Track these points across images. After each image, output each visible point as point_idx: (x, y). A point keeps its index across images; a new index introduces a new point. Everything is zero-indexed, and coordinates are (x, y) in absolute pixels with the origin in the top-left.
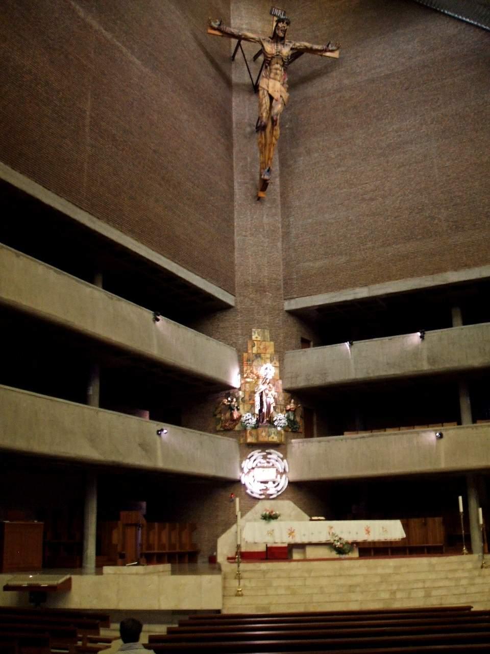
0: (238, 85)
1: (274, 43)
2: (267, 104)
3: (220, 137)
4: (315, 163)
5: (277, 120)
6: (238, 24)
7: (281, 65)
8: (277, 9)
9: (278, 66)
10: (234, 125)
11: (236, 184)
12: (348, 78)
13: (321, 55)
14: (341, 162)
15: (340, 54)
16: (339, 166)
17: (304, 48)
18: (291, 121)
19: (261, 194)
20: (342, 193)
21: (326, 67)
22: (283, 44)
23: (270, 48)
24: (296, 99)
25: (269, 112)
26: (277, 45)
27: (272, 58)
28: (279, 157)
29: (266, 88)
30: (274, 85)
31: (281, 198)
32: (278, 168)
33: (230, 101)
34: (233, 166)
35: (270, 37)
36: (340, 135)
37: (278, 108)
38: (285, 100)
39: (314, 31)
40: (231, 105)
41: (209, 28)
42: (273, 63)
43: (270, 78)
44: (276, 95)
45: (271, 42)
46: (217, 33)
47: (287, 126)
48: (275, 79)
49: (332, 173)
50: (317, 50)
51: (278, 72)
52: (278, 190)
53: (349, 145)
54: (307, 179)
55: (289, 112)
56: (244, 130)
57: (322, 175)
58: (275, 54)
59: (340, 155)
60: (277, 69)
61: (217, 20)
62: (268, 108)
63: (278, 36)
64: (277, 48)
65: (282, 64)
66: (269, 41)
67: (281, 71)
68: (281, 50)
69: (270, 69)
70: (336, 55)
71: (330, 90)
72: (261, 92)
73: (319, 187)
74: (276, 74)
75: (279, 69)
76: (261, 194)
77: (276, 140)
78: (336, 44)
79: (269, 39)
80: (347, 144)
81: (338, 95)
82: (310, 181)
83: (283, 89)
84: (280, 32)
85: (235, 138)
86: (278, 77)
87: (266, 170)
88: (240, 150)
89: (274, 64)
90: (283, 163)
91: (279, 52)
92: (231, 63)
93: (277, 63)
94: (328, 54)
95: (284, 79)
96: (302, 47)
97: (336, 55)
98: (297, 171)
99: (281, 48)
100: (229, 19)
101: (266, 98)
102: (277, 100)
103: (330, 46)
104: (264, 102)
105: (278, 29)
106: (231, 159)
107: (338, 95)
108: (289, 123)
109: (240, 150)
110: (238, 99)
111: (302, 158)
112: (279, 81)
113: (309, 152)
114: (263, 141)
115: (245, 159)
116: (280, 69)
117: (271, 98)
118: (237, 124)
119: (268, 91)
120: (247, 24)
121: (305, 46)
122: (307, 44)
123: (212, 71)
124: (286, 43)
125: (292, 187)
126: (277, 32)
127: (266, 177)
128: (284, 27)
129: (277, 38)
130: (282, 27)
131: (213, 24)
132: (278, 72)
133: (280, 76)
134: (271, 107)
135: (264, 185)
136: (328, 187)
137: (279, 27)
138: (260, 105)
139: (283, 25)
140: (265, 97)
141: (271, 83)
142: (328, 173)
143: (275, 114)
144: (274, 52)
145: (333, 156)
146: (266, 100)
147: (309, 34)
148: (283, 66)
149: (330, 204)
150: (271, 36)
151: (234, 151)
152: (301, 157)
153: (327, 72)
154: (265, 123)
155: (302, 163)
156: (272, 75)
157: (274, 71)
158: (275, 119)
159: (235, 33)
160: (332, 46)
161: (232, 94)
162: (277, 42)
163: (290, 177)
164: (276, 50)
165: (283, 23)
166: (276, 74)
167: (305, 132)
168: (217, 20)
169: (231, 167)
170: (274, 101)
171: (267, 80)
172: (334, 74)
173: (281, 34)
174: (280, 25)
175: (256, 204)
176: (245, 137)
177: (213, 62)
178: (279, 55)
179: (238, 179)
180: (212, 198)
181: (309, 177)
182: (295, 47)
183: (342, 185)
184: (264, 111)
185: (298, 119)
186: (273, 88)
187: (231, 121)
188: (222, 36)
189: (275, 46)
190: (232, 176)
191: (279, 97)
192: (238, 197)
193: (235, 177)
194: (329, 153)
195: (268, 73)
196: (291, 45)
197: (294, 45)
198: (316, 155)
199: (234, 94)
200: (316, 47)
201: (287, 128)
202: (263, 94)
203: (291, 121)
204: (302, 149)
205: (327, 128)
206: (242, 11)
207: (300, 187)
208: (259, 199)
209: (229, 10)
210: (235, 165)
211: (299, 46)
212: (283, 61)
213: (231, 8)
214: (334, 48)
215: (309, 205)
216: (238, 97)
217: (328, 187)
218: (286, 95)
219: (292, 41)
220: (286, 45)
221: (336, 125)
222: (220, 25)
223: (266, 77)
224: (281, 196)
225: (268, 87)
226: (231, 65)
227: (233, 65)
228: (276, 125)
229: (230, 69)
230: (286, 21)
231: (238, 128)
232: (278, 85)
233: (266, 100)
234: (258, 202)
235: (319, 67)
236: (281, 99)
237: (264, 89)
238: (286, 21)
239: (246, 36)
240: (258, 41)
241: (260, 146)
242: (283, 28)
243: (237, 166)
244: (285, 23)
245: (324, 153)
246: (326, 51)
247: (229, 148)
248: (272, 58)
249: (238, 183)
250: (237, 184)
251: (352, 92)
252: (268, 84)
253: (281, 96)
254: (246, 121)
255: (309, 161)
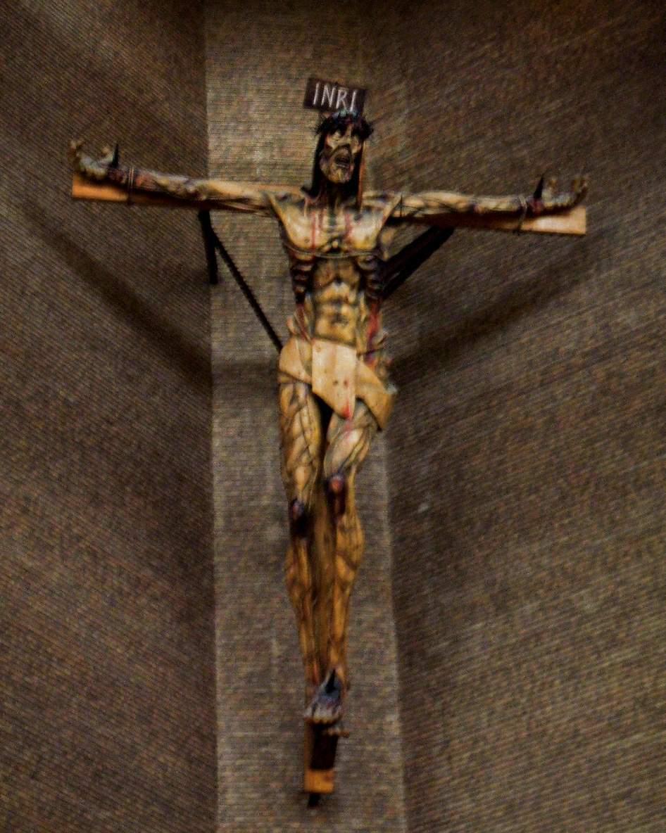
0: (233, 370)
1: (321, 206)
2: (308, 435)
3: (147, 573)
4: (525, 641)
5: (344, 491)
6: (235, 150)
7: (353, 287)
8: (331, 85)
9: (342, 290)
10: (219, 523)
11: (224, 748)
12: (631, 303)
13: (518, 231)
14: (619, 627)
15: (590, 219)
16: (614, 643)
17: (443, 211)
18: (437, 485)
19: (319, 782)
20: (625, 752)
21: (553, 272)
22: (356, 207)
23: (306, 228)
24: (453, 401)
25: (316, 463)
26: (333, 215)
27: (317, 262)
28: (398, 628)
29: (303, 375)
30: (336, 365)
31: (408, 789)
32: (393, 671)
33: (203, 434)
34: (211, 679)
35: (304, 189)
36: (613, 522)
37: (350, 442)
38: (377, 411)
39: (509, 145)
40: (208, 447)
41: (76, 178)
42: (321, 281)
43: (315, 335)
44: (341, 399)
45: (311, 207)
46: (107, 193)
47: (424, 507)
48: (334, 339)
49: (589, 675)
50: (493, 218)
51: (345, 310)
52: (396, 759)
53: (646, 558)
54: (499, 704)
55: (431, 453)
56: (258, 538)
57: (551, 684)
58: (327, 248)
59: (612, 600)
60: (338, 301)
61: (106, 150)
62: (313, 449)
63: (331, 184)
64: (333, 223)
65: (356, 279)
66: (300, 204)
67: (356, 304)
68: (348, 229)
69: (316, 305)
70: (575, 223)
71: (572, 354)
72: (286, 393)
73: (544, 733)
74: (337, 319)
75: (346, 301)
76: (319, 782)
77: (352, 566)
78: (573, 183)
79: (303, 196)
80: (639, 554)
81: (600, 372)
82: (509, 713)
83: (367, 372)
84: (334, 166)
85: (222, 573)
86: (346, 332)
87: (323, 686)
88: (241, 614)
89: (328, 284)
90: (414, 651)
91: (340, 238)
92: (207, 293)
93: (338, 280)
94: (543, 224)
95: (373, 335)
96: (429, 212)
97: (575, 223)
98: (462, 677)
99: (347, 222)
100: (202, 134)
101: (305, 411)
102: (344, 417)
103: (546, 194)
104: (297, 428)
105: (327, 158)
106: (206, 650)
107: (600, 372)
108: (428, 496)
109: (241, 614)
110: (235, 423)
111: (479, 625)
112: (353, 344)
113: (502, 601)
114: (306, 576)
115: (263, 645)
116: (352, 299)
117: (325, 410)
118: (228, 517)
119: (310, 386)
120: (268, 146)
121: (444, 206)
122: (451, 198)
123: (109, 325)
124: (366, 203)
125: (447, 743)
126: (324, 167)
127: (323, 714)
128: (347, 146)
129: (329, 192)
130: (339, 148)
131: (88, 163)
132: (345, 310)
133: (352, 325)
134: (324, 446)
135: (322, 747)
136: (576, 733)
137: (329, 147)
138: (286, 442)
139: (342, 141)
140: (299, 409)
141: (321, 354)
142: (574, 673)
143: (335, 468)
144: (320, 239)
145: (589, 607)
146: (307, 418)
147: (492, 157)
148: (361, 286)
149: (584, 798)
150: (308, 181)
151: (217, 620)
152: (474, 622)
153: (556, 292)
154: (305, 508)
155: (480, 642)
156: (323, 325)
157: (328, 309)
158: (335, 487)
159: (172, 188)
160: (556, 195)
161: (209, 407)
162: (332, 205)
163: (438, 705)
164: (330, 231)
165: (343, 134)
166: (337, 319)
167: (488, 524)
168: (106, 150)
169: (206, 686)
170: (334, 422)
171: (305, 345)
172: (583, 294)
173: (338, 175)
174: (333, 141)
175: (303, 818)
176: (262, 563)
177: (120, 299)
178: (338, 249)
179: (233, 729)
180: (104, 814)
181: (507, 698)
182: (406, 213)
183: (627, 721)
184: (298, 460)
185: (459, 477)
186: (328, 371)
187: (206, 506)
188: (129, 203)
189: (326, 219)
190: (212, 717)
191: (353, 400)
192: (231, 797)
193: (221, 723)
194: (573, 596)
195: (306, 320)
196: (388, 209)
197: (401, 205)
198: (529, 607)
199: (221, 408)
200: (489, 203)
201: (425, 513)
202: (294, 397)
203: (437, 485)
204: (476, 593)
205: (563, 498)
206: (249, 102)
207: (476, 741)
208: (315, 800)
209: (202, 103)
210: (220, 675)
211: (420, 209)
212: (357, 269)
213: (210, 95)
214: (564, 199)
215: (510, 808)
216: (235, 416)
217: (576, 733)
218: (379, 395)
219: (392, 194)
220: (369, 209)
221: (597, 485)
222: (114, 164)
223: (301, 335)
224: (407, 781)
225: (309, 369)
226: (209, 302)
227: (217, 302)
228: (343, 509)
229: (205, 317)
230: (350, 128)
231: (235, 532)
232: (347, 358)
233: (306, 420)
234: (313, 813)
235: (531, 273)
236: (362, 411)
237: (295, 380)
238: (350, 128)
239: (213, 192)
240: (261, 208)
241: (296, 595)
242: (345, 152)
243: (230, 671)
244: (349, 132)
245: (556, 598)
246: (532, 214)
247: (196, 610)
248: (317, 262)
249: (233, 743)
250: (228, 749)
251: (649, 354)
252: (311, 360)
253: (360, 400)
254: (265, 501)
255: (505, 636)
